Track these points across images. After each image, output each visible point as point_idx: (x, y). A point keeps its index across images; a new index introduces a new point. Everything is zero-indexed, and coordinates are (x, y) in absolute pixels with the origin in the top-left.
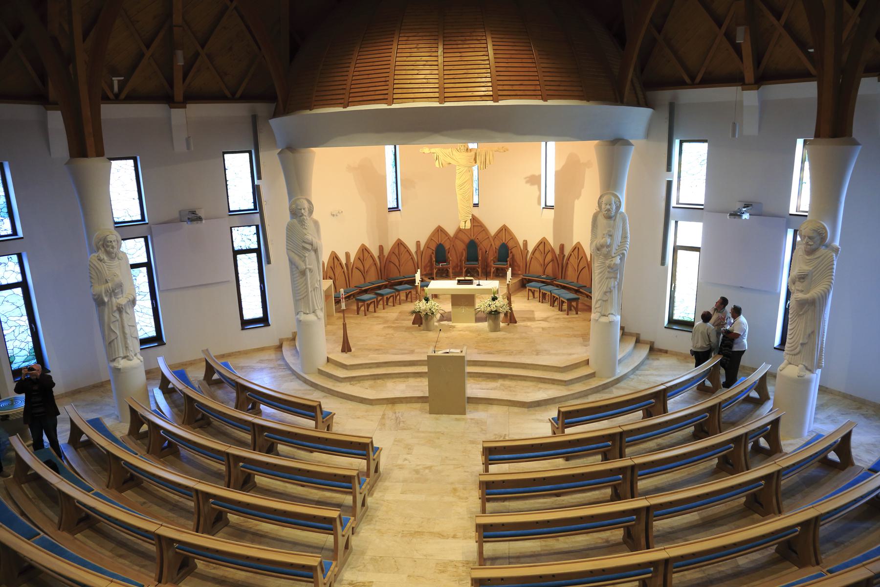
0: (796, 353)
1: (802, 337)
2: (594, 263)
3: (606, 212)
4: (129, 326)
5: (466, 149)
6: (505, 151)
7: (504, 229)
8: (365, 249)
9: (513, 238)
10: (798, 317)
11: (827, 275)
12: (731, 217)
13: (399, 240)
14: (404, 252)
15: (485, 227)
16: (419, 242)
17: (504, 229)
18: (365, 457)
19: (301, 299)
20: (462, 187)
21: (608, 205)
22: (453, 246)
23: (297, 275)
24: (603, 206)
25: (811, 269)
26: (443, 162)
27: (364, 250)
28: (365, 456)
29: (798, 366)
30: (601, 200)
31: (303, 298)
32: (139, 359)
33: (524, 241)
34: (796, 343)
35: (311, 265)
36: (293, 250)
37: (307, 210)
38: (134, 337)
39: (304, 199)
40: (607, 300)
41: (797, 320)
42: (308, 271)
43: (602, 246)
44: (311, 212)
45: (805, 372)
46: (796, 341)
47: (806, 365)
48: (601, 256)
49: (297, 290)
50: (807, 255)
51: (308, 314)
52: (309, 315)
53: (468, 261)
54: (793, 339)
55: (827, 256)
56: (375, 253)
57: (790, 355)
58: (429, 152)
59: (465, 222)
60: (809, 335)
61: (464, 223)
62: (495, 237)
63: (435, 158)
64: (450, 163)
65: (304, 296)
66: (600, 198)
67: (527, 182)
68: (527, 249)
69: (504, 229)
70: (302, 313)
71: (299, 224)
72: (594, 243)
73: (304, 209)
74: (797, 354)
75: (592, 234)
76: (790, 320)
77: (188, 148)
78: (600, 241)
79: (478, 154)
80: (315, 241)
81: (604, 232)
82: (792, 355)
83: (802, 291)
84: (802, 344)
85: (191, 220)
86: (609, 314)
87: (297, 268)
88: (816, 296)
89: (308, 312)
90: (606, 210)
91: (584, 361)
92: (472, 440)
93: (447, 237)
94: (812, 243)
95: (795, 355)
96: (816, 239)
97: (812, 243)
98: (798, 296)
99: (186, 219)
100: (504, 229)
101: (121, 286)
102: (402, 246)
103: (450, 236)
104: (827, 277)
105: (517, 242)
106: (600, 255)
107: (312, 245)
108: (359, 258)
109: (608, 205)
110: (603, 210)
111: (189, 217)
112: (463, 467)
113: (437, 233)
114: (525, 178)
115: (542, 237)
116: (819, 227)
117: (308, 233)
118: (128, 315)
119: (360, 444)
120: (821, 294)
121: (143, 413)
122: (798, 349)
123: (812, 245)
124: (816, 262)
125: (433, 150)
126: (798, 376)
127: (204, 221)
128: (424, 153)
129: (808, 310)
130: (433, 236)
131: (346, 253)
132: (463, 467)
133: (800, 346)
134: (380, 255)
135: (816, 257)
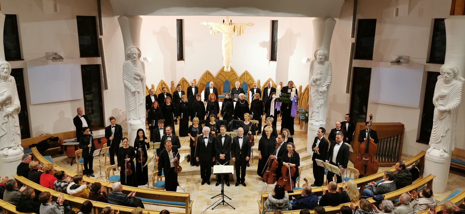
0: (438, 142)
1: (442, 132)
2: (310, 91)
3: (320, 60)
4: (15, 126)
5: (229, 23)
6: (252, 25)
7: (246, 74)
8: (163, 83)
9: (251, 78)
10: (440, 120)
11: (457, 96)
12: (392, 64)
13: (183, 78)
14: (186, 85)
15: (235, 72)
16: (195, 80)
17: (246, 74)
18: (185, 206)
19: (131, 111)
20: (226, 46)
21: (321, 56)
22: (216, 82)
23: (130, 95)
24: (318, 57)
25: (448, 92)
26: (215, 31)
27: (163, 84)
28: (185, 206)
29: (439, 150)
30: (316, 53)
31: (133, 110)
32: (21, 149)
33: (258, 80)
34: (439, 136)
35: (139, 89)
36: (127, 79)
37: (137, 55)
38: (17, 134)
39: (135, 48)
40: (319, 112)
41: (439, 122)
42: (136, 93)
43: (317, 80)
44: (139, 56)
45: (444, 153)
46: (439, 135)
47: (445, 149)
48: (315, 86)
49: (129, 105)
50: (446, 84)
51: (135, 120)
52: (137, 120)
53: (224, 93)
54: (436, 134)
55: (457, 84)
56: (169, 86)
57: (434, 143)
58: (206, 24)
59: (227, 67)
60: (447, 131)
61: (227, 68)
62: (241, 78)
63: (210, 28)
64: (219, 32)
65: (134, 108)
66: (316, 52)
67: (260, 46)
68: (259, 85)
69: (246, 74)
70: (132, 119)
71: (132, 63)
72: (312, 78)
73: (135, 54)
74: (440, 142)
75: (310, 73)
76: (434, 123)
77: (56, 10)
78: (315, 77)
79: (236, 27)
80: (142, 74)
81: (318, 72)
82: (436, 143)
83: (442, 105)
84: (442, 136)
85: (54, 59)
86: (320, 120)
87: (130, 90)
88: (451, 108)
89: (136, 119)
90: (320, 59)
91: (304, 148)
92: (245, 195)
93: (212, 78)
94: (449, 77)
95: (437, 143)
96: (451, 74)
97: (449, 77)
98: (440, 108)
99: (51, 58)
100: (246, 74)
101: (11, 99)
102: (185, 82)
103: (214, 77)
104: (458, 96)
105: (253, 81)
106: (315, 85)
107: (140, 77)
108: (159, 89)
109: (321, 56)
110: (318, 59)
111: (53, 57)
112: (244, 211)
113: (206, 75)
114: (260, 43)
115: (269, 78)
116: (453, 67)
117: (137, 69)
118: (14, 119)
119: (182, 197)
120: (455, 108)
121: (28, 183)
122: (439, 140)
123: (449, 78)
124: (451, 88)
125: (209, 24)
126: (440, 156)
127: (64, 60)
128: (203, 25)
129: (446, 116)
130: (204, 77)
131: (152, 85)
132: (244, 211)
133: (441, 138)
134: (172, 87)
135: (450, 85)
